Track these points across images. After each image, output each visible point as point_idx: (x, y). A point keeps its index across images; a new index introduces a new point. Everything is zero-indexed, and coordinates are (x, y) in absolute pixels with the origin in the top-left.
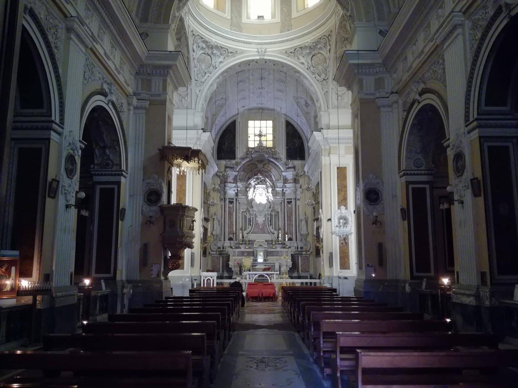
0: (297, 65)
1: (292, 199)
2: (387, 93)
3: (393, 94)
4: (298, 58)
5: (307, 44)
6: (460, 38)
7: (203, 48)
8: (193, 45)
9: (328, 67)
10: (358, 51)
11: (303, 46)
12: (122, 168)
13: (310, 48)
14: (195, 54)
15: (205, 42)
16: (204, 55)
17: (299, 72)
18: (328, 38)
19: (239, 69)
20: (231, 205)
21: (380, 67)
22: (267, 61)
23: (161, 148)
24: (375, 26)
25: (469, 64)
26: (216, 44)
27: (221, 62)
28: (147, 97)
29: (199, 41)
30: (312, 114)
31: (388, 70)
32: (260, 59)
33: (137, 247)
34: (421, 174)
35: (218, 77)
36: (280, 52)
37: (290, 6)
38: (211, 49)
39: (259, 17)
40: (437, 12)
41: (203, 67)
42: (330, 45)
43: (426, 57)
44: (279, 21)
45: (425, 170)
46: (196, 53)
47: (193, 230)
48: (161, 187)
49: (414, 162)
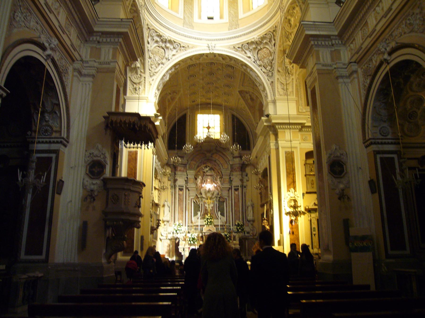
0: (244, 59)
1: (239, 186)
2: (344, 64)
3: (352, 64)
4: (245, 53)
5: (253, 40)
6: (356, 80)
7: (157, 42)
8: (148, 38)
9: (273, 60)
10: (314, 22)
11: (250, 41)
12: (63, 135)
13: (257, 43)
14: (149, 46)
15: (160, 36)
16: (158, 48)
17: (246, 65)
18: (273, 33)
19: (190, 62)
20: (181, 193)
21: (335, 39)
22: (217, 55)
23: (107, 115)
24: (328, 3)
25: (363, 99)
26: (169, 38)
27: (174, 55)
28: (96, 65)
29: (154, 34)
30: (257, 108)
31: (343, 43)
32: (210, 53)
33: (76, 225)
34: (388, 143)
35: (171, 69)
36: (229, 47)
37: (237, 9)
38: (166, 43)
39: (209, 18)
40: (349, 46)
41: (157, 59)
42: (274, 40)
43: (394, 14)
44: (227, 21)
45: (392, 139)
46: (150, 46)
47: (139, 207)
48: (105, 157)
49: (380, 131)
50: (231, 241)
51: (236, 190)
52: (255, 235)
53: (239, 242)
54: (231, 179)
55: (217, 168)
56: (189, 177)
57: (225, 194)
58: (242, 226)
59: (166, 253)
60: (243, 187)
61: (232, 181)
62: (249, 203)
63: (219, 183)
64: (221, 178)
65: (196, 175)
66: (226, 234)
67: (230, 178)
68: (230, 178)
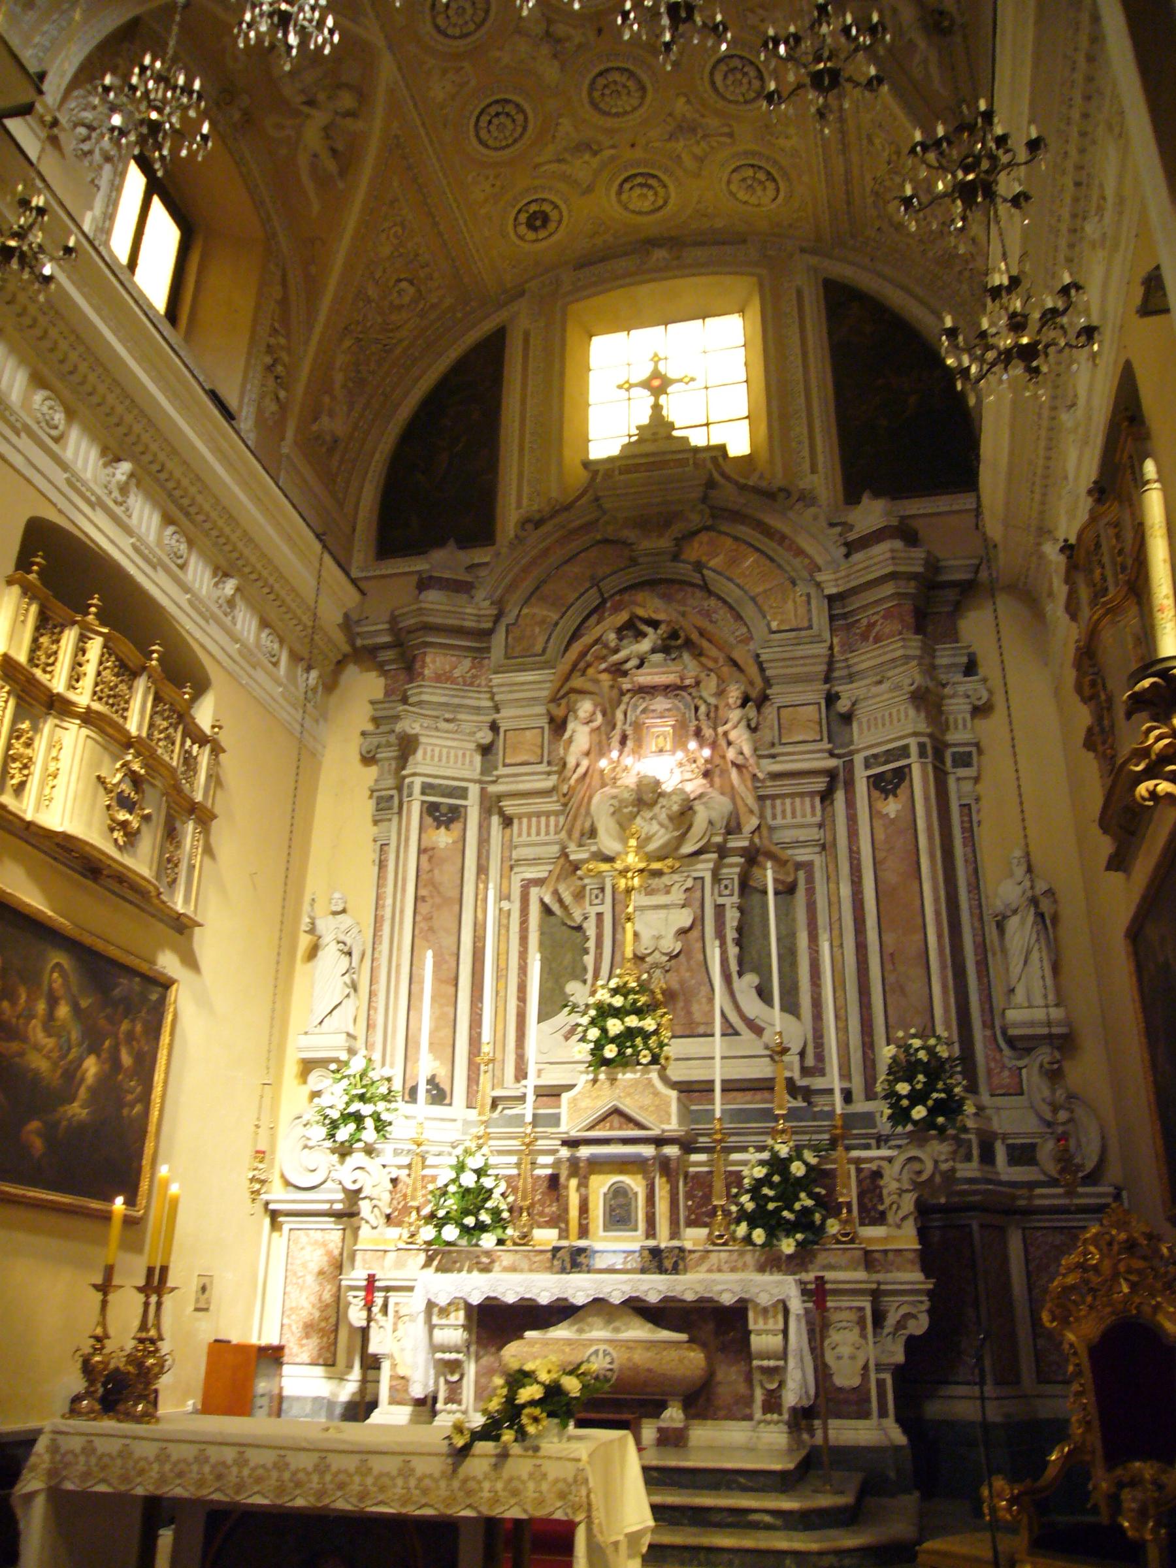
1: (904, 751)
20: (443, 838)
50: (833, 1227)
51: (888, 783)
52: (1093, 1178)
53: (923, 1233)
54: (843, 706)
55: (726, 628)
56: (507, 717)
57: (796, 822)
58: (935, 1069)
59: (309, 1328)
60: (937, 751)
61: (847, 718)
62: (1006, 890)
63: (740, 737)
64: (755, 700)
65: (555, 699)
66: (784, 1151)
67: (831, 699)
68: (831, 699)
